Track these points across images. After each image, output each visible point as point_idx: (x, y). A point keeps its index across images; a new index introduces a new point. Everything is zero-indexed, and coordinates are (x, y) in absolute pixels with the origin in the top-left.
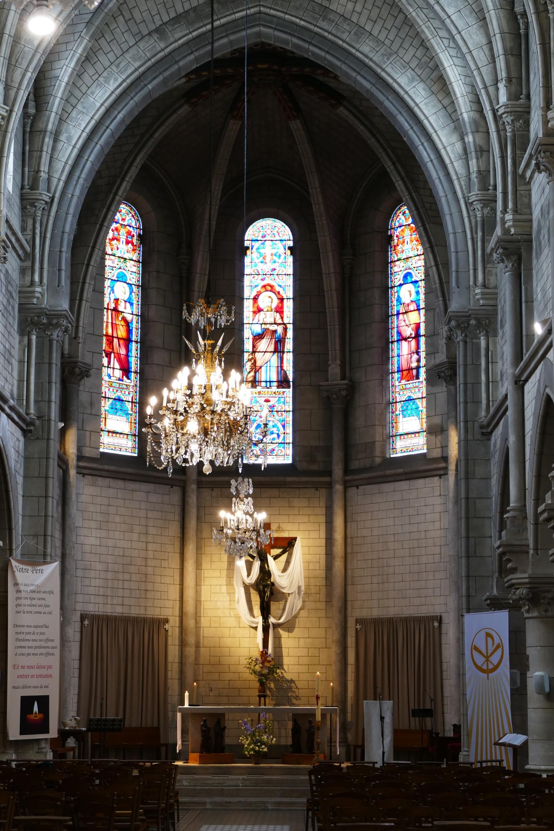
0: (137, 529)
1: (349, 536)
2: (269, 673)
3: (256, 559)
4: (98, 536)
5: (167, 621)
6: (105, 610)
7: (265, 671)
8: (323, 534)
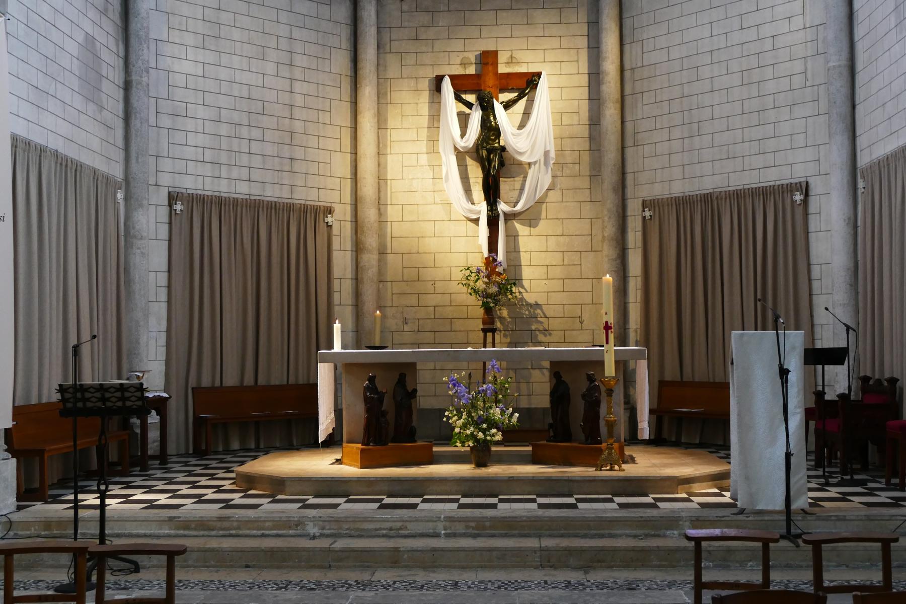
0: (272, 55)
1: (627, 66)
2: (499, 293)
3: (474, 107)
4: (200, 59)
5: (329, 211)
6: (216, 189)
7: (494, 289)
8: (584, 67)
